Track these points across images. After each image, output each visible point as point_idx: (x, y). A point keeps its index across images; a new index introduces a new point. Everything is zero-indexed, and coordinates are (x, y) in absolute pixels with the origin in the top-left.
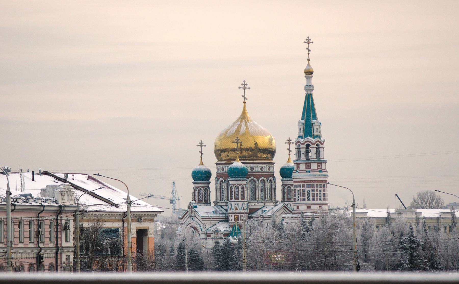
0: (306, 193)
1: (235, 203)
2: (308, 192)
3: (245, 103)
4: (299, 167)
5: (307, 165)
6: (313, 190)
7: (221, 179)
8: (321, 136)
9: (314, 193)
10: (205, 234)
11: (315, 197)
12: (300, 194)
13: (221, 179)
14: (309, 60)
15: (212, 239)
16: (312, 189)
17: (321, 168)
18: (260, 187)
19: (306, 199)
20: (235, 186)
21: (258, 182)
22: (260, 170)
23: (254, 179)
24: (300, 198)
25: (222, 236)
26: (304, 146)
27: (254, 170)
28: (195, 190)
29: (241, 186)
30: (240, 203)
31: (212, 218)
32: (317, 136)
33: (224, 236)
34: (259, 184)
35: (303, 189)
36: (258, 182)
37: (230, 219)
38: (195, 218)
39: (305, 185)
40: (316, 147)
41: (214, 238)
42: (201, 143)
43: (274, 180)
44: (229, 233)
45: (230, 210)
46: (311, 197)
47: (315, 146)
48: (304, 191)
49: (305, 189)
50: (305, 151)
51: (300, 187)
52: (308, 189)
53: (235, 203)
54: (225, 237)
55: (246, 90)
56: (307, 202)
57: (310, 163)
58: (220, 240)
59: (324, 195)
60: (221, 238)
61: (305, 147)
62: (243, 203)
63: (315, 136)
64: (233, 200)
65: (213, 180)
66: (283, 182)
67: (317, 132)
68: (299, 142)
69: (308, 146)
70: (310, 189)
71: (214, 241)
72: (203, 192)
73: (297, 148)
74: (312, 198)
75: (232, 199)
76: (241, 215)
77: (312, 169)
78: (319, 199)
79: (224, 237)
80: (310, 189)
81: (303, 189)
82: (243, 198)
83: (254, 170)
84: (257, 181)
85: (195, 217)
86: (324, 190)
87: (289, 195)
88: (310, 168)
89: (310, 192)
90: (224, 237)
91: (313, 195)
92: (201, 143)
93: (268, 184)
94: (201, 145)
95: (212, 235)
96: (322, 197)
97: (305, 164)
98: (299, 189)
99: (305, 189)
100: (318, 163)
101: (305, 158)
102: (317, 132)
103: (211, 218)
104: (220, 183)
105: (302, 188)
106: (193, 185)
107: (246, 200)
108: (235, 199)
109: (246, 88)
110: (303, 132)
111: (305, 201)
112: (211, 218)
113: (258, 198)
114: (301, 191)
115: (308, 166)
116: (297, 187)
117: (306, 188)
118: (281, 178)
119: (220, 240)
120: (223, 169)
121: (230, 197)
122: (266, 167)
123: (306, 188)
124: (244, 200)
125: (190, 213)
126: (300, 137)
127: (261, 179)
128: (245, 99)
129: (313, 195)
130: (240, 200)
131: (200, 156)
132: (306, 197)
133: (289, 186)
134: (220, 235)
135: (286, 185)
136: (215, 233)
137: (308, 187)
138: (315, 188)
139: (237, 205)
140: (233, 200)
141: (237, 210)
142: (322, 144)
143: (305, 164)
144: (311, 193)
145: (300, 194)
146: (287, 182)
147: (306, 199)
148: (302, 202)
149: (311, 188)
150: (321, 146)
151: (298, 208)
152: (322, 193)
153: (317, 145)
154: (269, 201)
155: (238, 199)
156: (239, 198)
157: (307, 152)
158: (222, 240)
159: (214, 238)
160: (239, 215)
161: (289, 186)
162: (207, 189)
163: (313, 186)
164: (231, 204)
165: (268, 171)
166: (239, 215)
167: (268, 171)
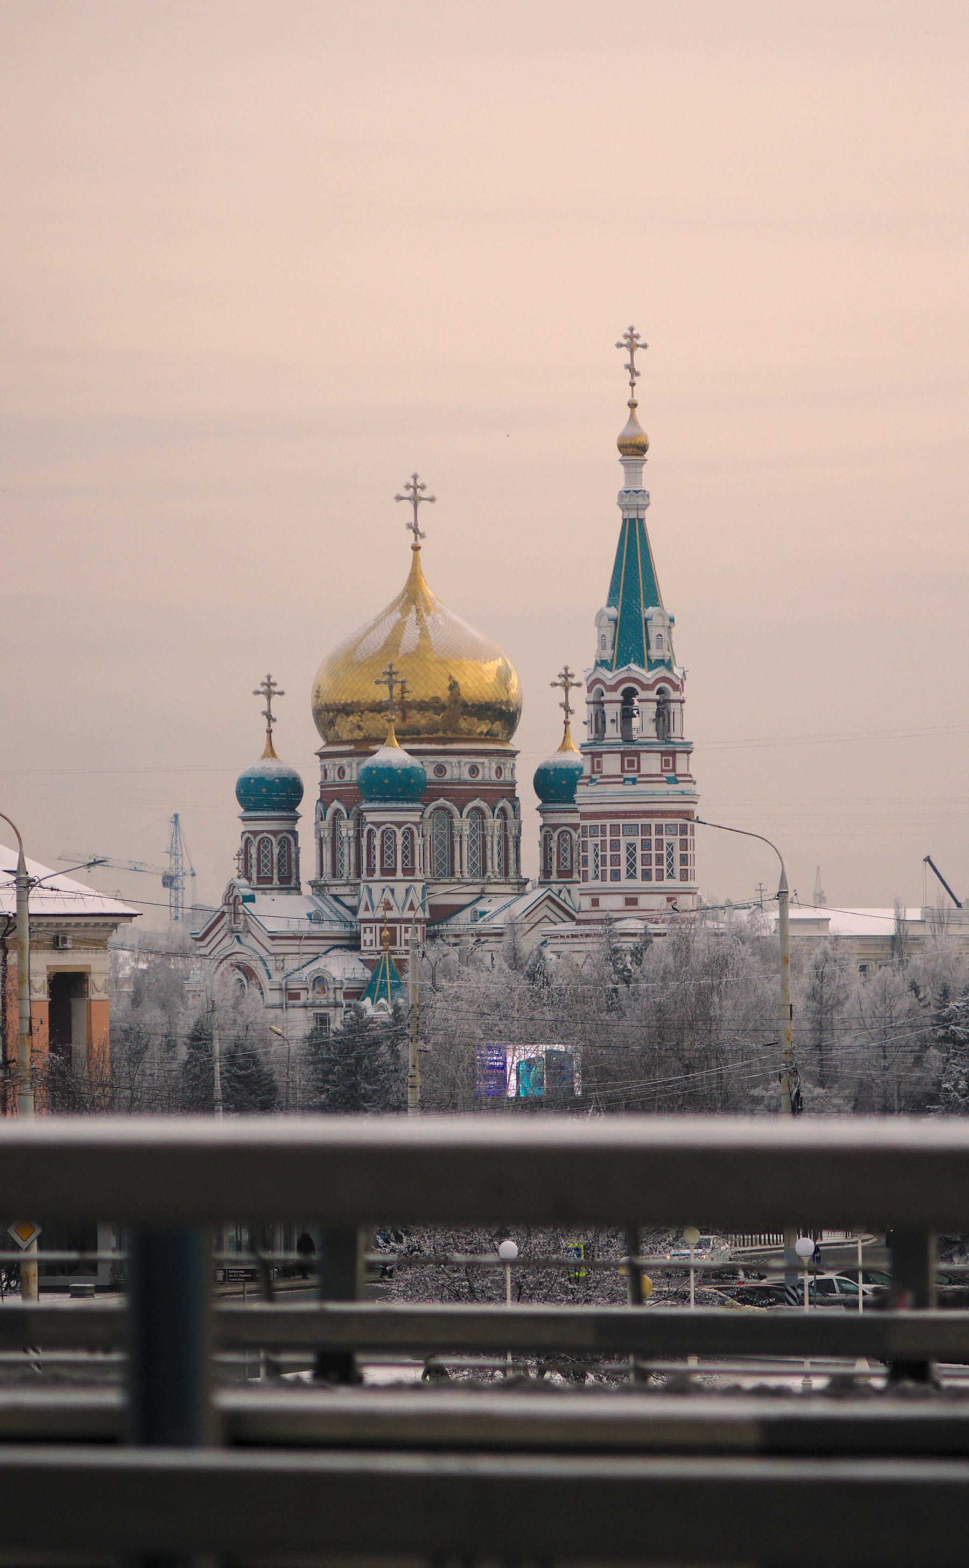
0: (623, 854)
1: (383, 885)
2: (628, 849)
3: (416, 548)
4: (599, 766)
5: (626, 759)
6: (646, 845)
7: (336, 805)
8: (672, 661)
9: (651, 854)
10: (281, 989)
11: (654, 867)
12: (604, 857)
13: (336, 805)
14: (633, 405)
15: (305, 1007)
16: (642, 840)
17: (674, 770)
18: (467, 831)
19: (623, 874)
20: (383, 828)
21: (461, 817)
22: (466, 776)
23: (448, 804)
24: (602, 871)
25: (340, 997)
26: (618, 696)
27: (447, 777)
28: (247, 842)
29: (402, 829)
30: (400, 888)
31: (307, 938)
32: (660, 662)
33: (345, 998)
34: (463, 824)
35: (611, 840)
36: (461, 817)
37: (365, 941)
38: (247, 937)
39: (619, 825)
40: (658, 697)
41: (313, 1006)
42: (269, 684)
43: (516, 809)
44: (363, 988)
45: (367, 909)
46: (639, 867)
47: (653, 695)
48: (615, 845)
49: (619, 840)
50: (619, 711)
51: (604, 833)
52: (631, 839)
53: (384, 887)
54: (348, 1001)
55: (422, 505)
56: (625, 883)
57: (637, 753)
58: (331, 1012)
59: (684, 859)
60: (337, 1005)
61: (621, 698)
62: (411, 886)
63: (653, 661)
64: (377, 875)
65: (308, 807)
66: (545, 815)
67: (659, 646)
68: (598, 681)
69: (629, 694)
70: (637, 840)
71: (311, 1014)
72: (276, 851)
73: (594, 703)
74: (642, 870)
75: (371, 872)
76: (404, 926)
77: (642, 772)
78: (665, 875)
79: (344, 1002)
80: (637, 840)
81: (611, 840)
82: (409, 871)
83: (447, 777)
84: (458, 813)
85: (249, 932)
86: (684, 845)
87: (565, 859)
88: (635, 768)
89: (635, 849)
90: (344, 1002)
91: (646, 860)
92: (269, 684)
93: (493, 823)
94: (269, 690)
95: (303, 994)
96: (677, 867)
97: (590, 756)
98: (598, 840)
99: (619, 840)
100: (663, 753)
101: (619, 735)
102: (659, 646)
103: (300, 938)
104: (334, 819)
105: (608, 838)
106: (241, 827)
107: (419, 875)
108: (384, 872)
109: (421, 499)
110: (613, 648)
111: (620, 880)
112: (300, 938)
113: (461, 868)
114: (606, 877)
115: (631, 763)
116: (592, 831)
117: (621, 838)
118: (539, 802)
119: (331, 1012)
120: (341, 772)
121: (365, 866)
122: (487, 764)
123: (621, 838)
124: (413, 875)
125: (230, 921)
126: (602, 663)
127: (471, 805)
128: (418, 536)
129: (646, 860)
130: (399, 875)
131: (266, 726)
132: (623, 867)
133: (564, 828)
134: (331, 995)
135: (555, 827)
136: (314, 989)
137: (631, 830)
138: (654, 837)
139: (388, 894)
140: (377, 875)
141: (391, 909)
142: (676, 688)
143: (619, 756)
144: (639, 853)
145: (602, 871)
146: (559, 817)
147: (623, 874)
148: (609, 884)
149: (640, 837)
150: (674, 695)
151: (595, 903)
152: (677, 853)
153: (660, 692)
154: (496, 880)
155: (393, 871)
156: (272, 878)
157: (627, 715)
158: (339, 1009)
159: (313, 1006)
160: (395, 928)
161: (564, 828)
162: (289, 840)
163: (646, 829)
164: (370, 891)
165: (494, 777)
166: (398, 926)
167: (494, 777)
